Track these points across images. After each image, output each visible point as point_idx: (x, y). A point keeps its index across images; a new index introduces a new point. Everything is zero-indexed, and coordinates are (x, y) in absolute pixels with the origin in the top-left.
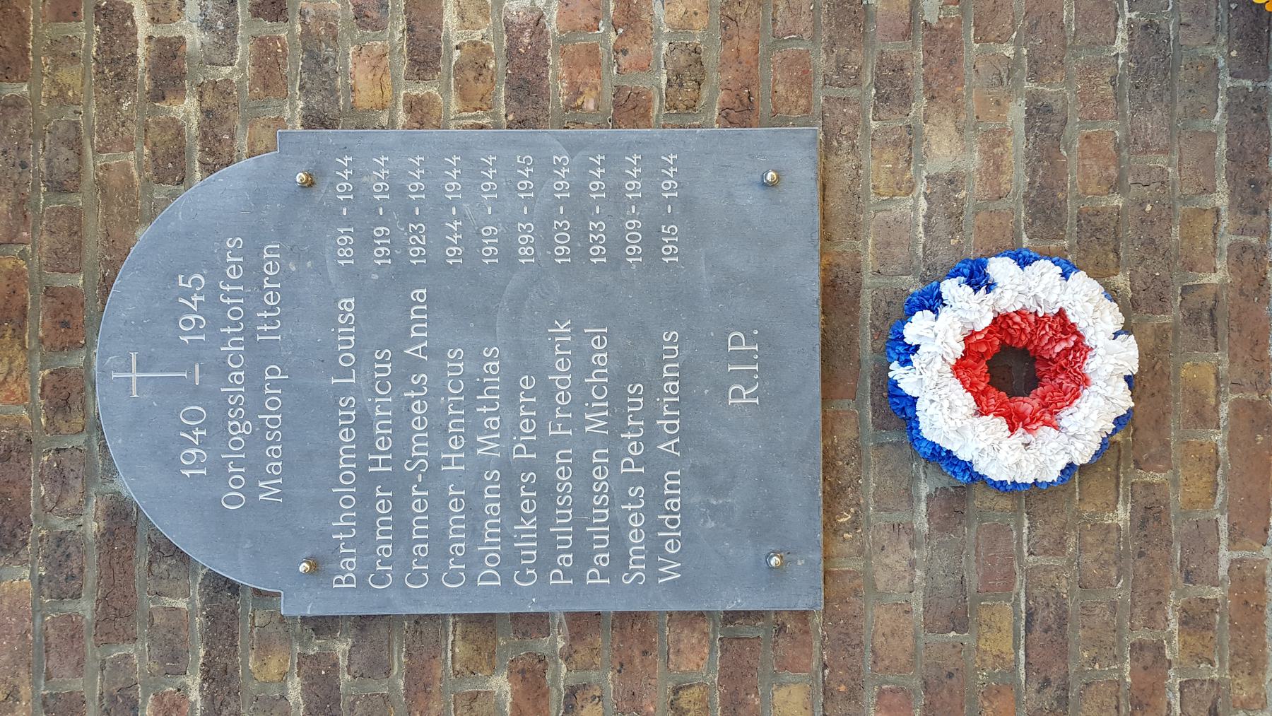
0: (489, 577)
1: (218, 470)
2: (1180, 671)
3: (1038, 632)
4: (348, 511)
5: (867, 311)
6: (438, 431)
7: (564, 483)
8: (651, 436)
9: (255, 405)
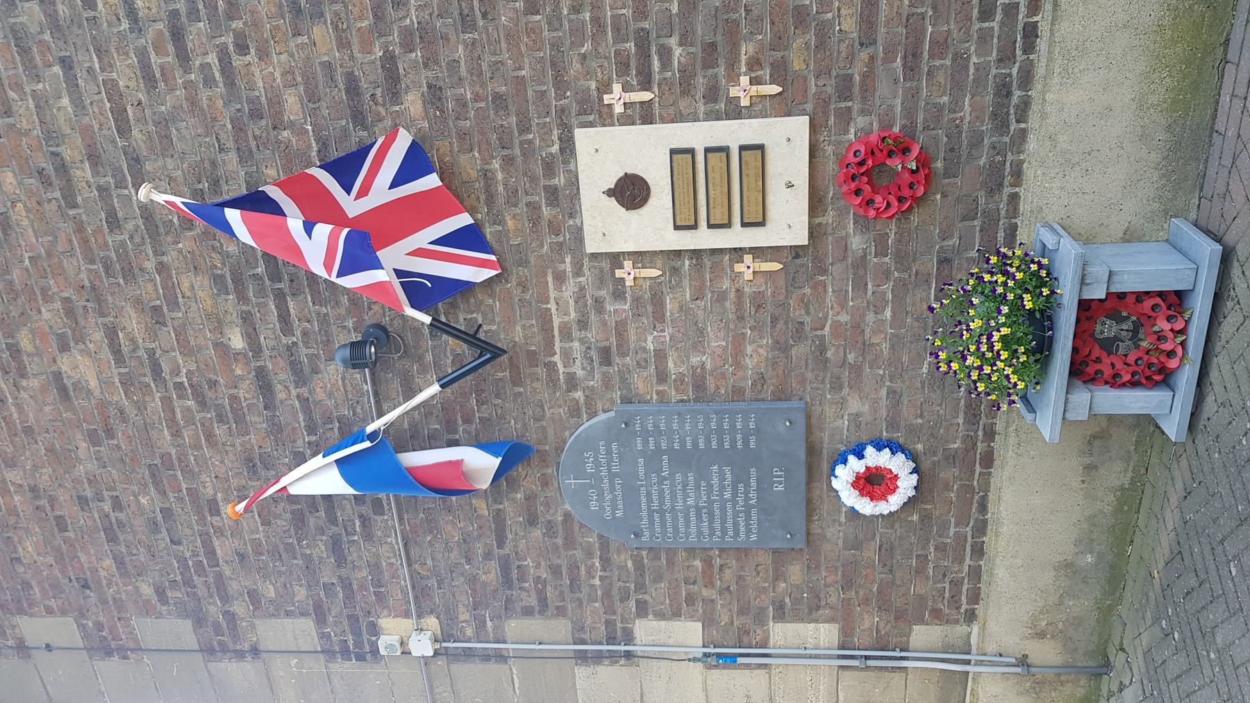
0: (693, 538)
1: (602, 508)
2: (933, 562)
3: (883, 550)
4: (646, 519)
5: (825, 456)
6: (674, 498)
7: (717, 512)
8: (747, 499)
9: (612, 489)
